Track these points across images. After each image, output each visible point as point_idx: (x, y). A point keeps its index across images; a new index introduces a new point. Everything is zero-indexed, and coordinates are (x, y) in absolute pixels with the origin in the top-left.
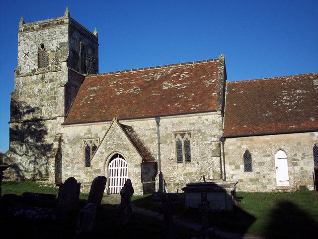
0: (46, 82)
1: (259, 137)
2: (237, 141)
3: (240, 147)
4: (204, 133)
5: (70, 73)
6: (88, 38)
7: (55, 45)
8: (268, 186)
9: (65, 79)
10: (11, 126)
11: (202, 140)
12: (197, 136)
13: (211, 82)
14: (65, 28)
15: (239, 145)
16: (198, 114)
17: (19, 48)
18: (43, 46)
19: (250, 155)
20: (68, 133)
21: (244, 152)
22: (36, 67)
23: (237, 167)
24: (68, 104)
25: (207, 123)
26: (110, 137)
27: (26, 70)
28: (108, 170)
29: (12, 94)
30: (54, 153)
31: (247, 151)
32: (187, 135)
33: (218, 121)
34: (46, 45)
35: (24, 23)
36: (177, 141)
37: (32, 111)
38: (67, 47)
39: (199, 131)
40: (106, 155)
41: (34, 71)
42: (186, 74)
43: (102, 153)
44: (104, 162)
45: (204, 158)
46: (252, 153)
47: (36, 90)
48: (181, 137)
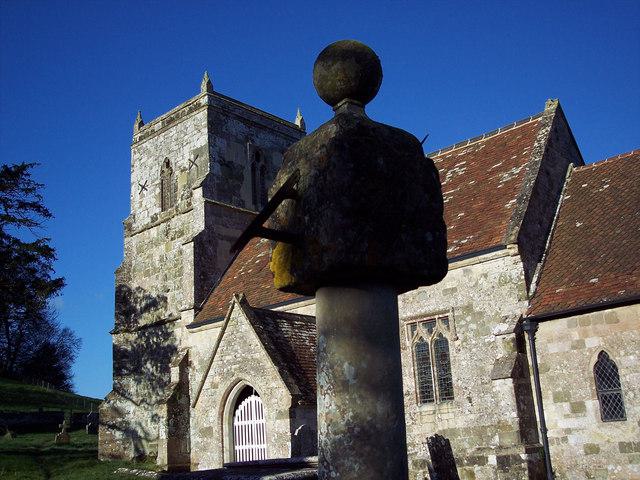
0: (172, 239)
1: (633, 307)
2: (569, 326)
3: (579, 345)
4: (481, 314)
5: (211, 210)
6: (272, 131)
7: (187, 156)
9: (198, 224)
10: (115, 339)
11: (477, 334)
12: (463, 323)
13: (512, 174)
14: (202, 116)
15: (576, 335)
16: (459, 263)
17: (134, 178)
18: (168, 163)
19: (614, 366)
21: (595, 359)
23: (578, 408)
24: (204, 280)
25: (485, 284)
27: (142, 219)
28: (232, 428)
29: (118, 272)
30: (169, 393)
31: (603, 355)
33: (514, 276)
34: (172, 161)
35: (141, 124)
36: (436, 341)
37: (153, 304)
38: (206, 157)
39: (468, 308)
41: (154, 219)
42: (461, 167)
44: (217, 408)
45: (484, 388)
47: (157, 258)
48: (425, 330)
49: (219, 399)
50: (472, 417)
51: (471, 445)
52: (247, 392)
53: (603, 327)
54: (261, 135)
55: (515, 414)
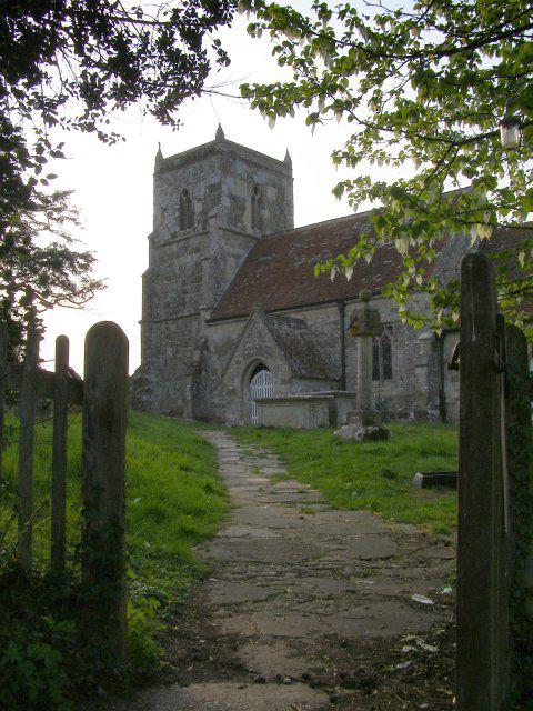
6: (267, 169)
7: (203, 190)
11: (410, 338)
22: (177, 229)
32: (386, 330)
40: (244, 365)
41: (174, 236)
43: (238, 363)
44: (240, 378)
49: (241, 372)
52: (261, 367)
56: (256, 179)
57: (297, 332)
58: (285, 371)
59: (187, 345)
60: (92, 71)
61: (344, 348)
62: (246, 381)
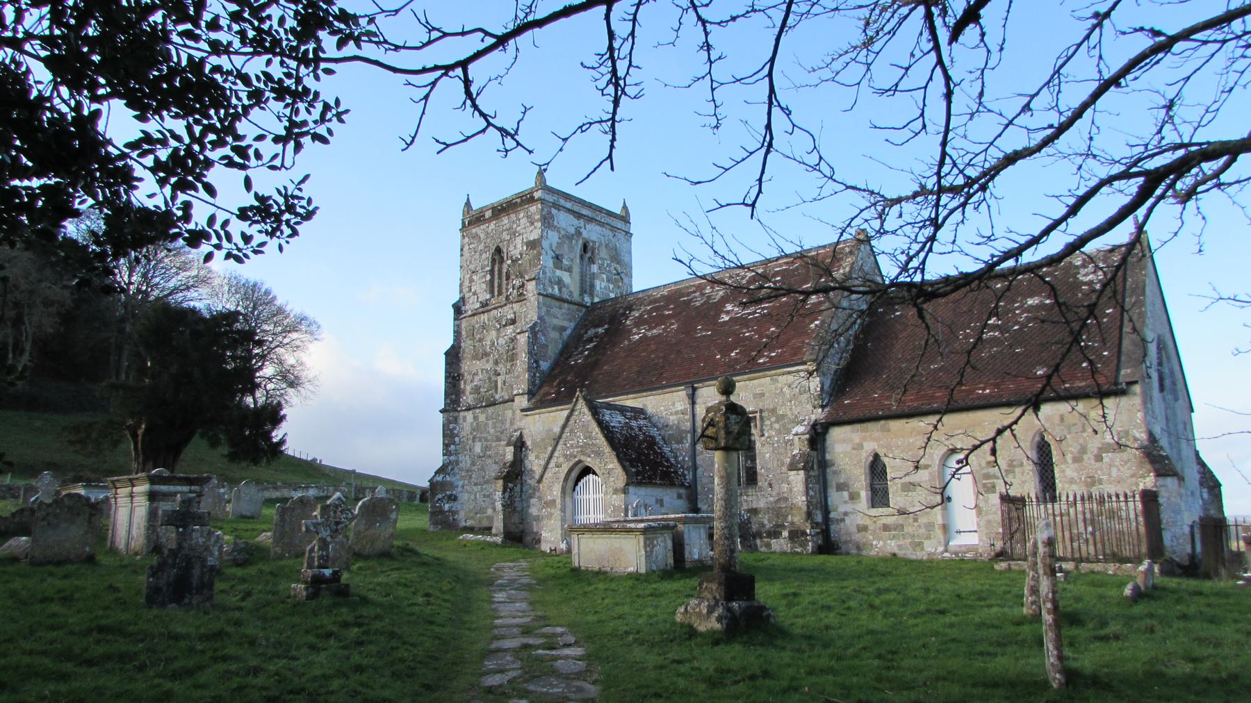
4: (783, 416)
7: (519, 246)
8: (926, 543)
15: (857, 440)
18: (498, 251)
20: (532, 428)
25: (788, 392)
26: (571, 431)
39: (774, 411)
40: (565, 468)
41: (484, 304)
46: (886, 460)
49: (563, 476)
50: (771, 499)
51: (770, 521)
52: (587, 471)
53: (876, 434)
54: (589, 227)
55: (804, 498)
56: (585, 234)
57: (634, 423)
58: (619, 476)
59: (499, 439)
60: (758, 415)
61: (611, 48)
62: (569, 490)
